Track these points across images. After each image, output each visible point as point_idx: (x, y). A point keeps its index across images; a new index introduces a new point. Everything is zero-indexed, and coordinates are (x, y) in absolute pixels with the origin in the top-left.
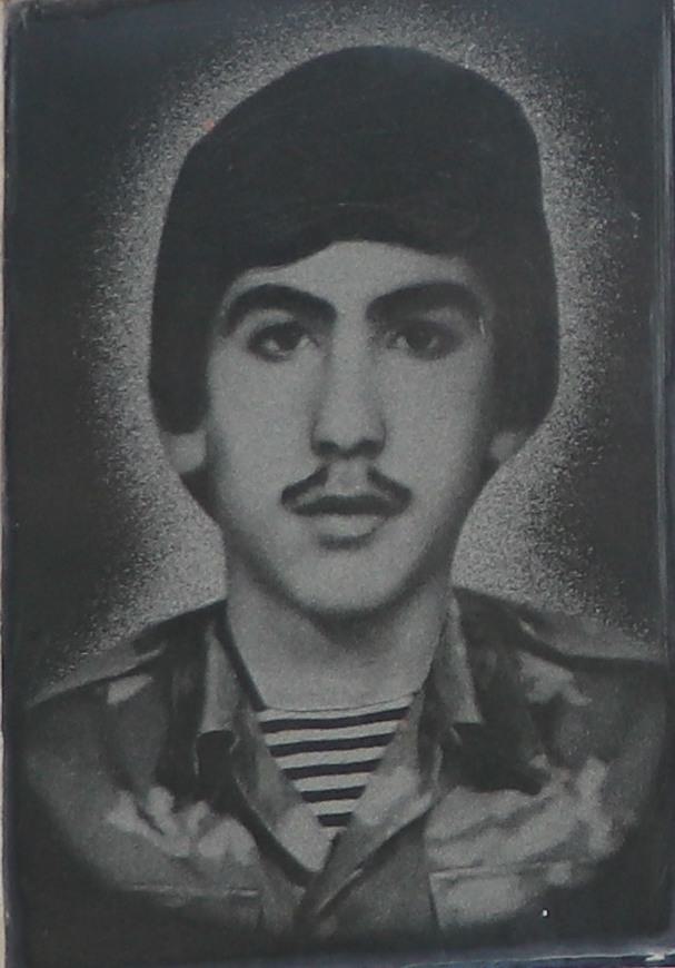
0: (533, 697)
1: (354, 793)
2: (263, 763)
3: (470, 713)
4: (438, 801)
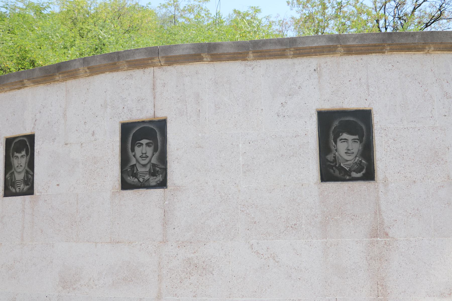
0: (157, 170)
1: (145, 177)
2: (16, 185)
3: (152, 171)
4: (150, 177)
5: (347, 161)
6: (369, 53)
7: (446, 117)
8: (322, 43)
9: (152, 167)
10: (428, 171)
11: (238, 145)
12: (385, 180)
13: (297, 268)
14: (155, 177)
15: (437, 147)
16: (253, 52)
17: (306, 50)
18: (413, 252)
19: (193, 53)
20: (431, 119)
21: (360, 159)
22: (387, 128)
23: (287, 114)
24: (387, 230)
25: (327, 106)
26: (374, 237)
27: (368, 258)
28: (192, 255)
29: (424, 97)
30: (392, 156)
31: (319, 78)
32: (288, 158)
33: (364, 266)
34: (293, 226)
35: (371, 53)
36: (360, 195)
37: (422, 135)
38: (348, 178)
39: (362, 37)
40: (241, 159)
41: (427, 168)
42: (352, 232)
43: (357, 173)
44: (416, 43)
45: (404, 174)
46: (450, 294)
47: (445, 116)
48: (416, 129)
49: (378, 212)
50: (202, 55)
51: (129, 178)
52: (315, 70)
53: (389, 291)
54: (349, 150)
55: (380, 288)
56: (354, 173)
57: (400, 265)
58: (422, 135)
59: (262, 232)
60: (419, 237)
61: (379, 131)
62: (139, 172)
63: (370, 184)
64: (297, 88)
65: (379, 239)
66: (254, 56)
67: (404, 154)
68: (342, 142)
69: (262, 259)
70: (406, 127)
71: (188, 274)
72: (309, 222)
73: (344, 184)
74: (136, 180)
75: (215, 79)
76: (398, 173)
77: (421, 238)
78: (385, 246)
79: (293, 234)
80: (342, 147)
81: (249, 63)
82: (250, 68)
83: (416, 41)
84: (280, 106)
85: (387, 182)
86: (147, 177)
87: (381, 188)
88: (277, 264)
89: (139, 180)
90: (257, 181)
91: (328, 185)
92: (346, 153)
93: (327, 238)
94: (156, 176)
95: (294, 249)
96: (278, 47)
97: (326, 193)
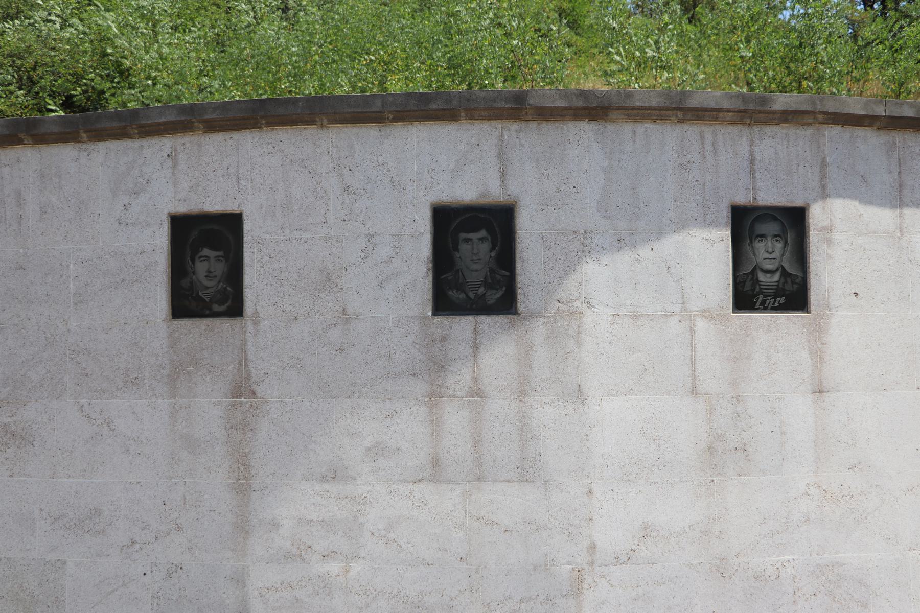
1: (477, 290)
3: (490, 281)
5: (207, 288)
6: (242, 129)
7: (346, 222)
8: (171, 117)
9: (489, 274)
10: (315, 303)
11: (68, 266)
12: (256, 314)
13: (136, 438)
14: (494, 292)
15: (330, 268)
16: (86, 132)
17: (360, 111)
18: (288, 419)
19: (7, 133)
20: (323, 225)
21: (225, 286)
22: (262, 240)
23: (131, 221)
24: (254, 387)
25: (182, 209)
26: (237, 398)
27: (228, 426)
28: (9, 420)
29: (315, 193)
30: (266, 281)
31: (174, 167)
32: (130, 284)
33: (222, 437)
34: (133, 380)
35: (245, 129)
36: (222, 337)
37: (309, 250)
38: (207, 312)
39: (224, 107)
40: (71, 286)
41: (315, 298)
42: (209, 389)
43: (220, 305)
44: (299, 114)
45: (282, 306)
46: (334, 478)
47: (344, 220)
48: (302, 241)
49: (243, 362)
50: (19, 135)
51: (450, 293)
52: (168, 156)
53: (253, 472)
54: (210, 272)
55: (242, 468)
56: (216, 306)
57: (269, 437)
58: (309, 250)
59: (95, 388)
60: (298, 397)
61: (250, 245)
62: (468, 282)
63: (236, 321)
64: (144, 183)
65: (243, 400)
66: (88, 137)
67: (284, 278)
68: (201, 261)
69: (94, 426)
70: (287, 237)
71: (4, 446)
72: (154, 375)
73: (201, 322)
74: (462, 296)
75: (41, 170)
76: (274, 305)
77: (300, 399)
78: (251, 410)
79: (134, 392)
80: (201, 268)
81: (84, 146)
82: (86, 154)
83: (299, 111)
84: (123, 208)
85: (258, 318)
86: (481, 290)
87: (250, 327)
88: (112, 432)
89: (467, 295)
90: (91, 317)
91: (180, 322)
92: (206, 276)
93: (177, 398)
94: (497, 289)
95: (134, 413)
96: (115, 124)
97: (177, 335)
